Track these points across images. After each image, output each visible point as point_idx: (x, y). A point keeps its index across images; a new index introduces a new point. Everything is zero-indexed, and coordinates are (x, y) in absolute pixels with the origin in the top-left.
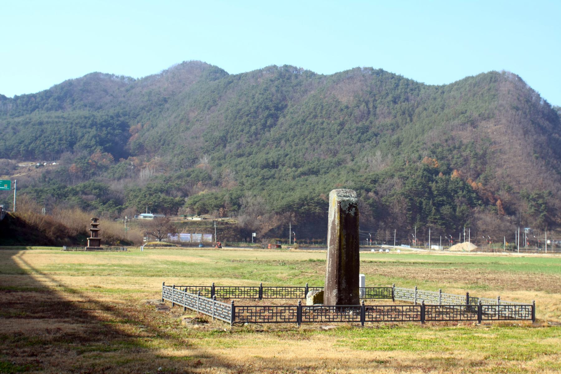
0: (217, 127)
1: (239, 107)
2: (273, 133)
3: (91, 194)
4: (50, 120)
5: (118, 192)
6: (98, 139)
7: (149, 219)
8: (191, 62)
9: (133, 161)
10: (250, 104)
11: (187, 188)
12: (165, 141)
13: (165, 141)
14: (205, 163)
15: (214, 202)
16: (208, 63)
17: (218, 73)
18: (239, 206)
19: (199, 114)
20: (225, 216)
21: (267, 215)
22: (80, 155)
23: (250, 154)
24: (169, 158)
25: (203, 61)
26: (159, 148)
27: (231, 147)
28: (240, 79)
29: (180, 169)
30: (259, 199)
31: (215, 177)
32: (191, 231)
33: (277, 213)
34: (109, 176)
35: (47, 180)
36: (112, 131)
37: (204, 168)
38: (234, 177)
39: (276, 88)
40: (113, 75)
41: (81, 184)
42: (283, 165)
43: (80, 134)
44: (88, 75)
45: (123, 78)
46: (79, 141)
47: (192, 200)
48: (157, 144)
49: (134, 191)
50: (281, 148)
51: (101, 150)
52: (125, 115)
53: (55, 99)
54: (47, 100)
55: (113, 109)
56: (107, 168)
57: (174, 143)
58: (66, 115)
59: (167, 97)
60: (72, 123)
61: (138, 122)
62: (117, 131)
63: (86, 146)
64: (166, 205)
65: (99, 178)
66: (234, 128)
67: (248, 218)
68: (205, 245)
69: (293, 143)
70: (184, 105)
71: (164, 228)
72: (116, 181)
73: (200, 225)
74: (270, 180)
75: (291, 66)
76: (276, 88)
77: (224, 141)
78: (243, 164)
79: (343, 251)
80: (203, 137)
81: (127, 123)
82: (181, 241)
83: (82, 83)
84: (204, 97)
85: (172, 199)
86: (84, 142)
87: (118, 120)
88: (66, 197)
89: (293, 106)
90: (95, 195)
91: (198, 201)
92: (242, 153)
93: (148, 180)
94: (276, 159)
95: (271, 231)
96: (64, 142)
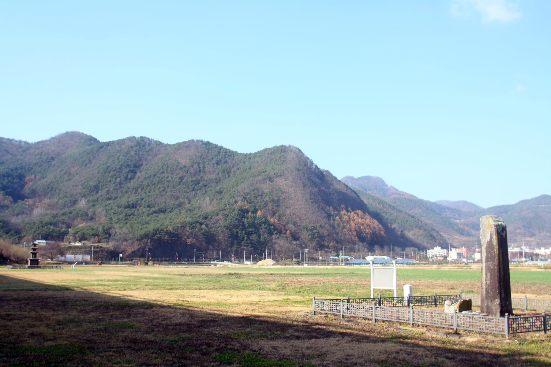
1: (108, 165)
2: (133, 184)
5: (17, 225)
9: (28, 202)
10: (116, 163)
11: (70, 222)
12: (52, 188)
15: (91, 232)
18: (110, 235)
21: (130, 241)
23: (116, 198)
24: (55, 200)
25: (81, 131)
27: (102, 193)
31: (90, 214)
33: (137, 240)
36: (12, 180)
40: (13, 140)
42: (140, 206)
45: (20, 142)
49: (30, 224)
52: (22, 169)
56: (7, 207)
59: (54, 156)
61: (32, 174)
67: (117, 243)
68: (87, 263)
74: (132, 216)
75: (145, 137)
77: (97, 189)
87: (16, 172)
89: (146, 165)
94: (135, 202)
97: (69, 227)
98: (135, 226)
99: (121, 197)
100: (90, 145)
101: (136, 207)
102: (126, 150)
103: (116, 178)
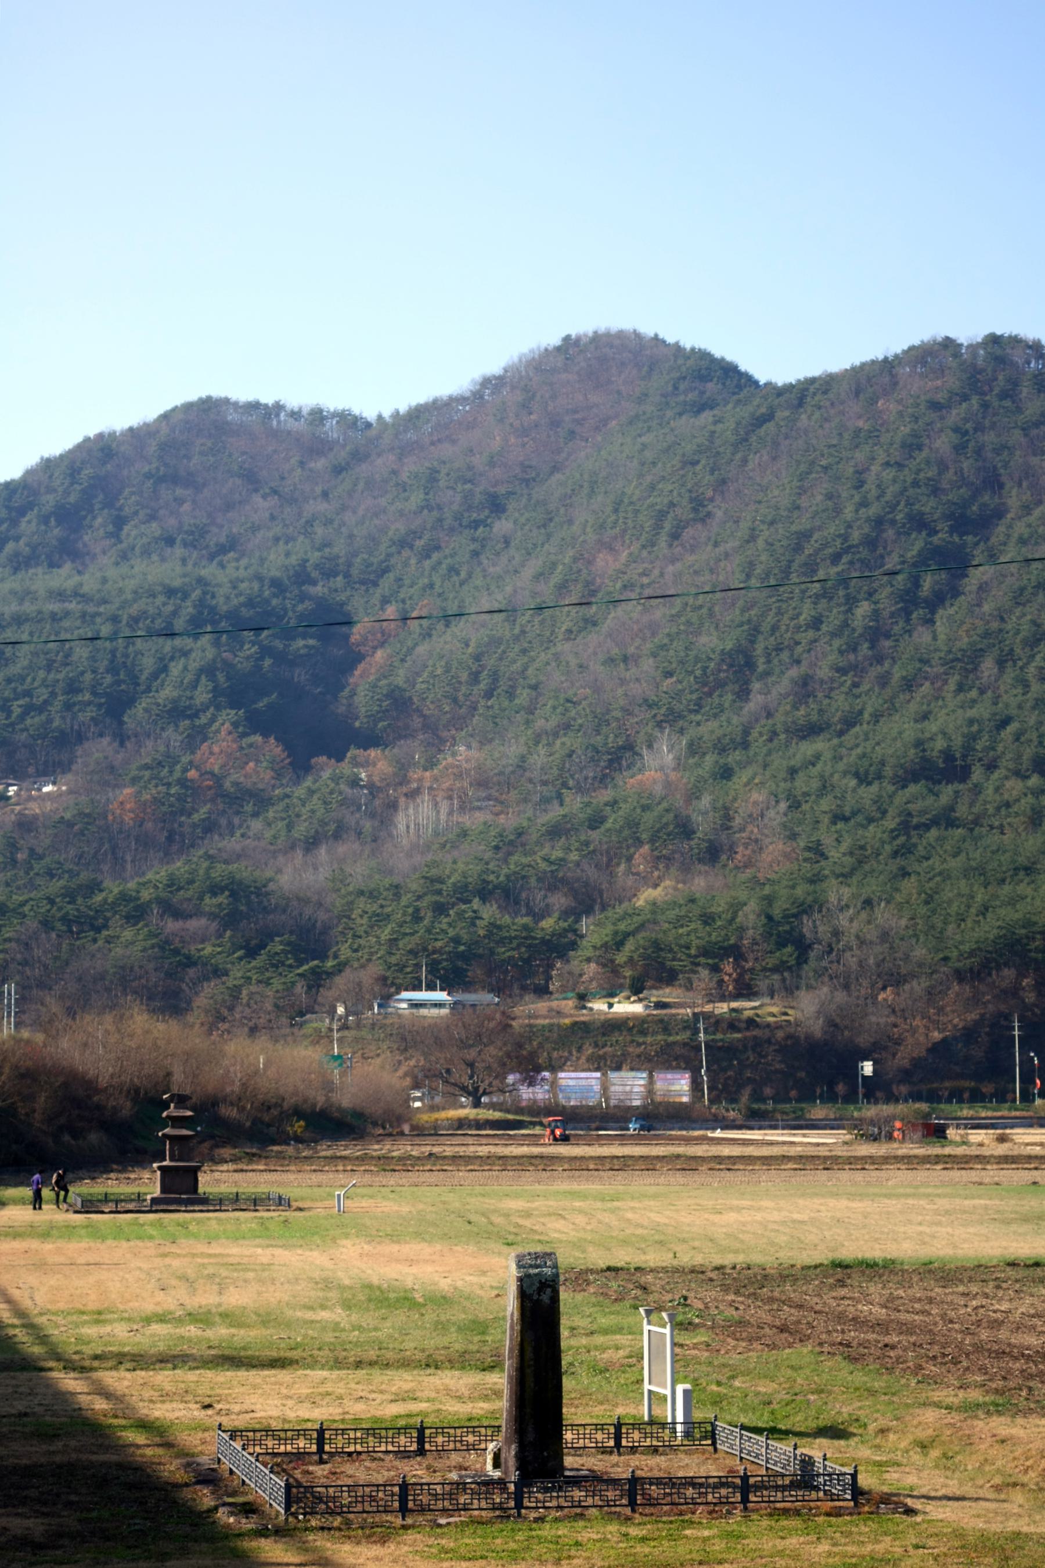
0: (711, 614)
1: (803, 523)
2: (948, 629)
3: (198, 913)
4: (29, 608)
5: (307, 901)
6: (221, 677)
7: (435, 1012)
8: (598, 340)
9: (366, 764)
10: (848, 513)
11: (591, 873)
12: (495, 677)
13: (495, 677)
14: (662, 769)
15: (697, 935)
16: (670, 339)
17: (712, 379)
18: (803, 948)
19: (633, 559)
20: (745, 990)
21: (918, 986)
22: (150, 750)
23: (850, 721)
24: (513, 750)
25: (648, 330)
26: (474, 708)
27: (770, 693)
28: (801, 403)
29: (560, 797)
30: (883, 915)
31: (704, 824)
32: (603, 1057)
33: (960, 976)
34: (268, 834)
35: (20, 856)
36: (278, 644)
37: (658, 790)
38: (784, 826)
39: (955, 438)
40: (278, 407)
41: (158, 873)
42: (991, 767)
43: (148, 663)
44: (175, 409)
45: (318, 415)
46: (149, 690)
47: (609, 929)
48: (463, 689)
49: (372, 895)
50: (982, 692)
51: (235, 725)
52: (329, 574)
53: (45, 520)
54: (14, 523)
55: (282, 547)
56: (261, 801)
57: (534, 687)
58: (89, 583)
59: (502, 490)
60: (115, 619)
61: (385, 601)
62: (301, 643)
63: (177, 712)
64: (503, 952)
65: (232, 844)
66: (780, 612)
67: (841, 997)
68: (656, 1117)
69: (1032, 669)
70: (570, 522)
71: (493, 1052)
72: (299, 853)
73: (643, 1033)
74: (934, 833)
75: (1015, 341)
76: (955, 438)
77: (740, 668)
78: (819, 766)
79: (528, 1371)
80: (654, 655)
81: (342, 604)
82: (563, 1101)
83: (152, 448)
84: (652, 487)
85: (525, 927)
86: (167, 693)
87: (303, 597)
88: (98, 930)
89: (1027, 509)
90: (212, 916)
91: (633, 933)
92: (814, 717)
93: (428, 847)
94: (958, 741)
95: (936, 1049)
96: (87, 697)
97: (587, 901)
98: (948, 893)
99: (876, 717)
100: (700, 408)
101: (962, 774)
102: (905, 430)
103: (851, 602)
